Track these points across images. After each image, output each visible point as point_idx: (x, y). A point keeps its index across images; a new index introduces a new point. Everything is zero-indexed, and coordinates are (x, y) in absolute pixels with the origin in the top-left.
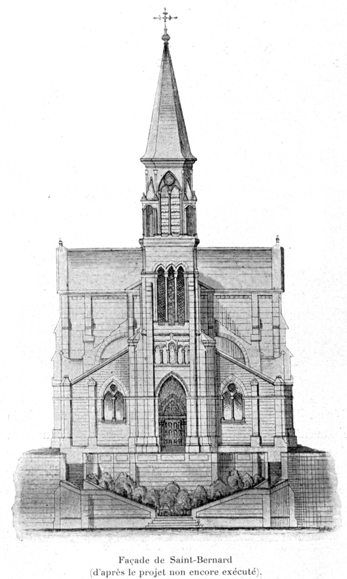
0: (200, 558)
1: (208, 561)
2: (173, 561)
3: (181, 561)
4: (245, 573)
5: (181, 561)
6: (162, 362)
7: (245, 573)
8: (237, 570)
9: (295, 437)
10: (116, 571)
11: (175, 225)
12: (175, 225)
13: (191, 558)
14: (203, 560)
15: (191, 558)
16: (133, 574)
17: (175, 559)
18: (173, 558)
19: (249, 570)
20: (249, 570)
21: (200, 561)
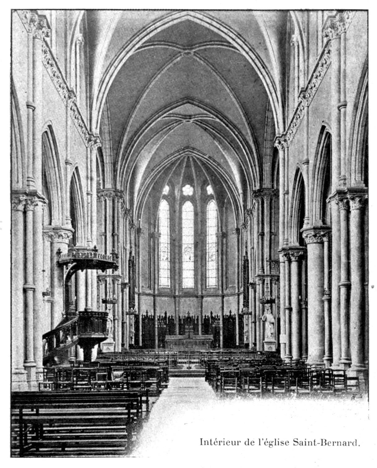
0: (324, 441)
1: (332, 443)
2: (296, 443)
3: (304, 444)
4: (234, 443)
5: (304, 444)
6: (250, 390)
7: (234, 443)
8: (218, 440)
9: (217, 237)
10: (223, 440)
11: (323, 16)
12: (323, 16)
13: (315, 441)
14: (327, 442)
15: (315, 441)
16: (253, 444)
17: (299, 441)
18: (296, 440)
19: (211, 441)
20: (211, 441)
21: (324, 444)
